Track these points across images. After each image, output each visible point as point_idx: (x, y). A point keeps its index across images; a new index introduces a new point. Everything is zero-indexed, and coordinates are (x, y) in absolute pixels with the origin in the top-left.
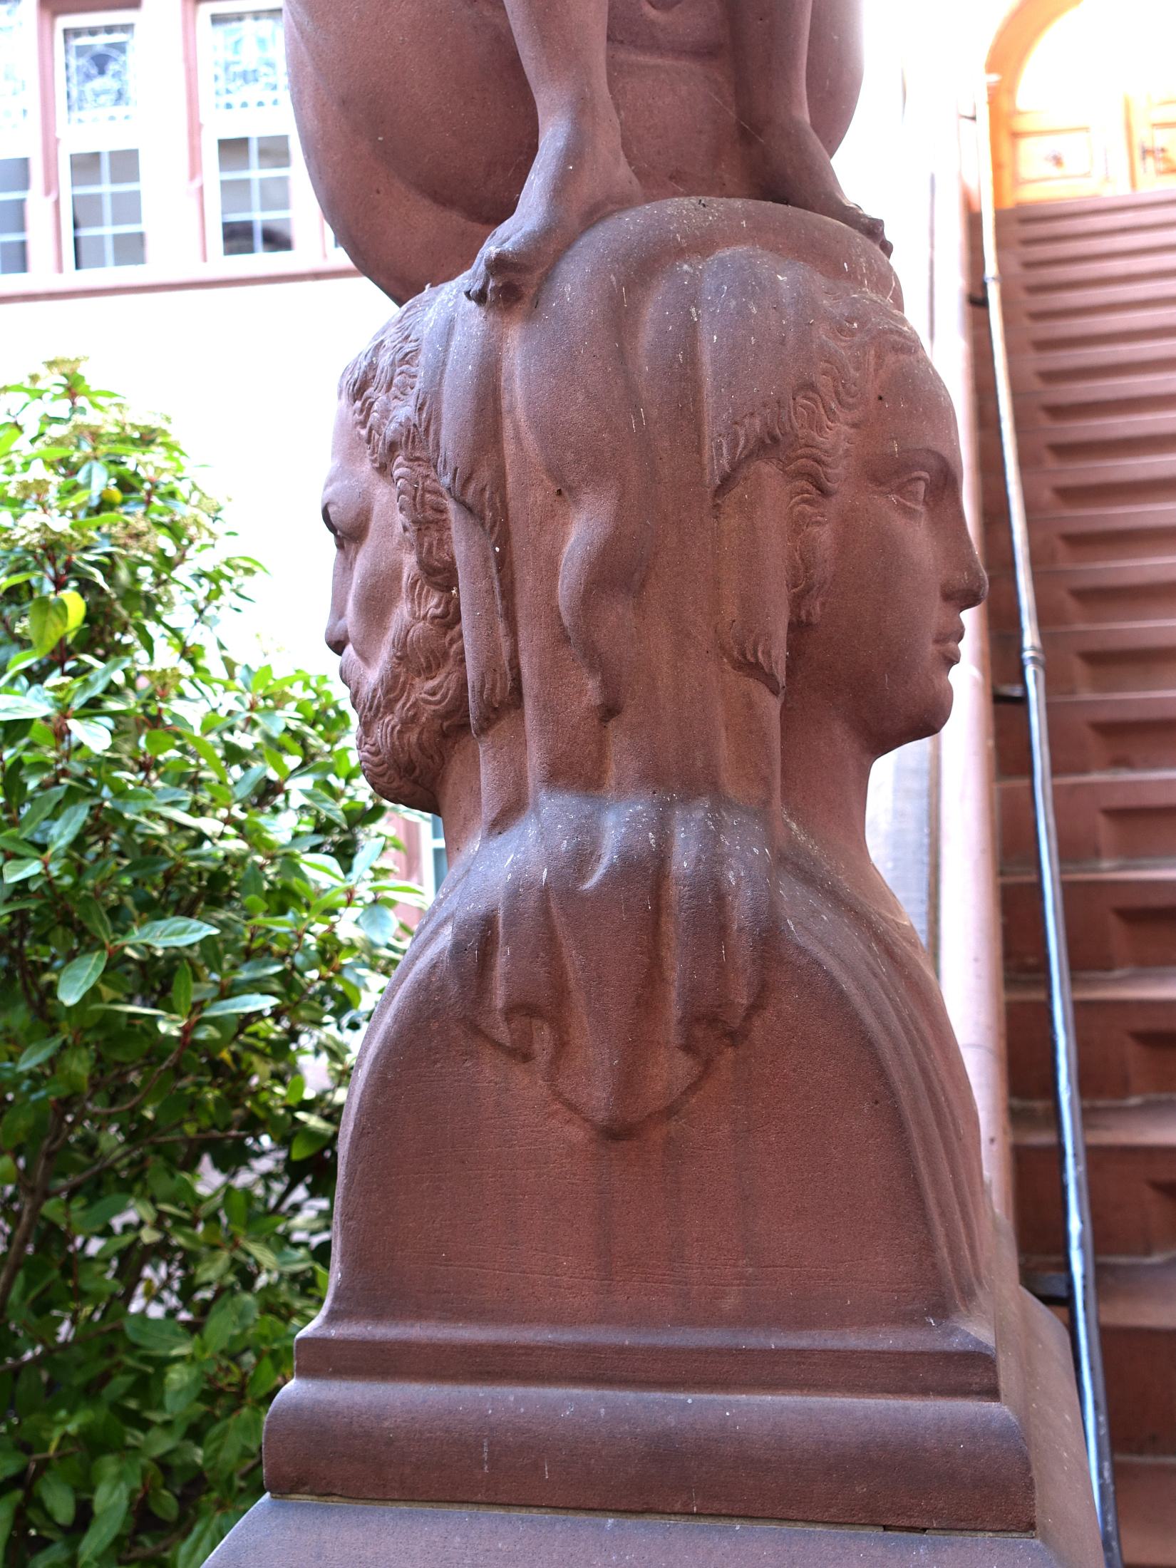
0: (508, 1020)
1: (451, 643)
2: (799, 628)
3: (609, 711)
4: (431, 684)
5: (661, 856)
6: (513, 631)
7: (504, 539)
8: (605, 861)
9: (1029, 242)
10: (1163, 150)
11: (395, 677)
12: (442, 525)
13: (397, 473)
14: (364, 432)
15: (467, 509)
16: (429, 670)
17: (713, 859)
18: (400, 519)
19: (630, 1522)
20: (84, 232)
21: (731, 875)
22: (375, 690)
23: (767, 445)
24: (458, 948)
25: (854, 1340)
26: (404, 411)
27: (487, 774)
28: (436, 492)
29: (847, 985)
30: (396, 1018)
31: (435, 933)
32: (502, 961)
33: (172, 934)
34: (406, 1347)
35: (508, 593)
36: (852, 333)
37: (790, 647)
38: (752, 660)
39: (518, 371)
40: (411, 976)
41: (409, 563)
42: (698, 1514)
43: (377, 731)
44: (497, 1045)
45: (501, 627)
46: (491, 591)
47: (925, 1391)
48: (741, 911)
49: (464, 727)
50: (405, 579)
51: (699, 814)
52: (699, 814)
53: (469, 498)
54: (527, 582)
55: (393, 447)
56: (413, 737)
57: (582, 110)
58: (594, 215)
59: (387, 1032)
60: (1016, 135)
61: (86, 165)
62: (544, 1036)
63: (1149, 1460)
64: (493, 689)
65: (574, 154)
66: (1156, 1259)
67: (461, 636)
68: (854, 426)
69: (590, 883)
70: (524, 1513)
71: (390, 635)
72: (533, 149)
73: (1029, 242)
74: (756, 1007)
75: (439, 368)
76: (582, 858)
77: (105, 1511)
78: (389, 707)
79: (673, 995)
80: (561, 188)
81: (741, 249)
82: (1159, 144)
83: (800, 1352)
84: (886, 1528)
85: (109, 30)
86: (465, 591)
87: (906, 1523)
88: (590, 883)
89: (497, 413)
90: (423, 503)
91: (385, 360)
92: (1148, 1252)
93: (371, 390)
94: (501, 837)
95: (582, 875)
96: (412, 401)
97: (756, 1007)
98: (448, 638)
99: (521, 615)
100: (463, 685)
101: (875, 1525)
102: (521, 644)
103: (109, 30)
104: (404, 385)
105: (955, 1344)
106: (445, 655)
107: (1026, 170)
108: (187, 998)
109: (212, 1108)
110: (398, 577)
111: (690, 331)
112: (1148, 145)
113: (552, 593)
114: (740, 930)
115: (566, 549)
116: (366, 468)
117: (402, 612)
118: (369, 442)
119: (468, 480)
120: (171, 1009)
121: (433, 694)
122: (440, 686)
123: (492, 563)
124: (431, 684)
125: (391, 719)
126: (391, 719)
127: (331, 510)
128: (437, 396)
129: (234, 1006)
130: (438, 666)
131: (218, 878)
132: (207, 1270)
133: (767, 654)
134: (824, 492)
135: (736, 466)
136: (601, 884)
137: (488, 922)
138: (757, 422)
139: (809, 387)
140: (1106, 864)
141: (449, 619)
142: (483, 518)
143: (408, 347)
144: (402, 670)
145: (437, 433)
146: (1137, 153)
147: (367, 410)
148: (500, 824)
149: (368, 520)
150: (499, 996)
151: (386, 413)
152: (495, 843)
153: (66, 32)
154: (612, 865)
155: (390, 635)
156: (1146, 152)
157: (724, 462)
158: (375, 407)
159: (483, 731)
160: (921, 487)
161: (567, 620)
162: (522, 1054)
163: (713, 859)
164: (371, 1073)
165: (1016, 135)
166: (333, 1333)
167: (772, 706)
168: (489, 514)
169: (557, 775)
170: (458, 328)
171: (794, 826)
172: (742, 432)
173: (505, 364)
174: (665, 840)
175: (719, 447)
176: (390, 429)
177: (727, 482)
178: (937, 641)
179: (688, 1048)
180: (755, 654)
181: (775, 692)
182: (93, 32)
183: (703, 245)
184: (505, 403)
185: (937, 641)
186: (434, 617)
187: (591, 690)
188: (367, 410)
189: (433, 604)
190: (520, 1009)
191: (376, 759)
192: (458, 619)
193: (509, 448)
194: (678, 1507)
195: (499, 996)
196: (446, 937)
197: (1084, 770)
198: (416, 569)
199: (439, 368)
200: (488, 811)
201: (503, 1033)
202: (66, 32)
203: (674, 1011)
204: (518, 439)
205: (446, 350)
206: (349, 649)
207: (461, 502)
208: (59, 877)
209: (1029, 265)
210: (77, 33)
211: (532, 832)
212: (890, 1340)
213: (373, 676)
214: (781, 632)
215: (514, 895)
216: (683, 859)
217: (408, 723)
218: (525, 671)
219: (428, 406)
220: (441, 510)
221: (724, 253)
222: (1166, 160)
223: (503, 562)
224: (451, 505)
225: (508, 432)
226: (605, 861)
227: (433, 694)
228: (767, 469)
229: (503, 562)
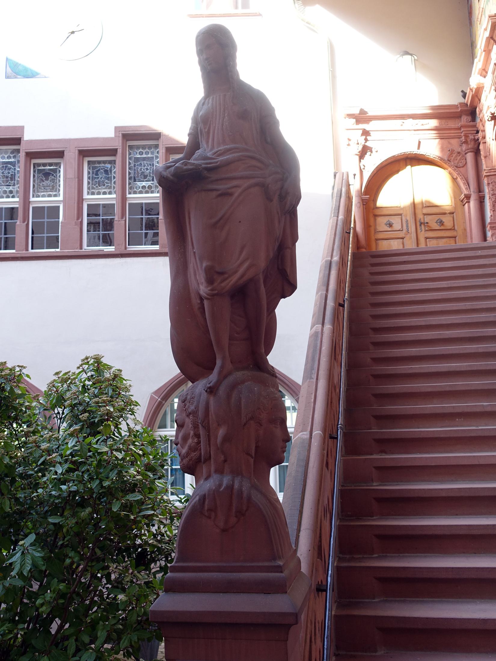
0: (207, 512)
1: (199, 447)
2: (257, 447)
3: (225, 461)
4: (195, 453)
5: (233, 486)
6: (210, 447)
7: (209, 432)
8: (224, 486)
9: (373, 265)
10: (427, 223)
11: (188, 452)
12: (198, 428)
13: (191, 418)
14: (184, 409)
15: (203, 426)
16: (194, 451)
17: (241, 486)
18: (191, 426)
19: (225, 594)
20: (34, 235)
21: (244, 489)
22: (184, 454)
23: (252, 418)
24: (200, 500)
25: (260, 564)
26: (192, 408)
27: (205, 470)
28: (198, 422)
29: (261, 507)
30: (189, 511)
31: (195, 497)
32: (206, 503)
33: (133, 497)
34: (188, 567)
35: (209, 441)
36: (267, 398)
37: (255, 450)
38: (248, 453)
39: (212, 405)
40: (191, 505)
41: (192, 433)
42: (236, 592)
43: (184, 461)
44: (205, 516)
45: (208, 446)
46: (206, 440)
47: (271, 572)
48: (245, 495)
49: (200, 461)
50: (191, 435)
51: (239, 478)
52: (239, 478)
53: (203, 425)
54: (212, 439)
55: (190, 414)
56: (191, 463)
57: (224, 358)
58: (225, 377)
59: (187, 514)
60: (376, 216)
61: (38, 211)
62: (213, 514)
63: (369, 654)
64: (206, 456)
65: (222, 367)
66: (376, 600)
67: (201, 446)
68: (267, 413)
69: (222, 489)
70: (208, 593)
71: (188, 445)
72: (215, 364)
73: (373, 265)
74: (247, 510)
75: (198, 402)
76: (220, 485)
77: (99, 637)
78: (187, 457)
79: (234, 508)
80: (220, 373)
81: (249, 383)
82: (426, 221)
83: (252, 566)
84: (265, 593)
85: (50, 164)
86: (202, 439)
87: (267, 592)
88: (222, 489)
89: (208, 410)
90: (195, 423)
91: (189, 397)
92: (374, 599)
93: (186, 402)
94: (207, 481)
95: (220, 488)
96: (194, 406)
97: (247, 510)
98: (198, 446)
99: (211, 444)
100: (201, 454)
101: (263, 593)
102: (211, 449)
103: (50, 164)
104: (192, 403)
105: (276, 564)
106: (198, 449)
107: (380, 228)
108: (136, 511)
109: (132, 538)
110: (190, 435)
111: (240, 399)
112: (422, 221)
113: (216, 441)
114: (245, 498)
115: (219, 434)
116: (184, 415)
117: (190, 441)
118: (185, 411)
119: (203, 422)
120: (132, 514)
121: (195, 455)
122: (196, 454)
123: (207, 435)
124: (195, 453)
125: (187, 459)
126: (187, 459)
127: (177, 421)
128: (198, 406)
129: (145, 513)
130: (196, 451)
131: (135, 485)
132: (126, 579)
133: (251, 452)
134: (261, 425)
135: (247, 422)
136: (223, 490)
137: (205, 495)
138: (250, 415)
139: (259, 409)
140: (375, 484)
141: (199, 443)
142: (205, 428)
143: (193, 396)
144: (189, 451)
145: (198, 413)
146: (418, 224)
147: (185, 405)
148: (206, 479)
149: (184, 424)
150: (206, 507)
151: (189, 407)
152: (206, 482)
153: (34, 164)
154: (225, 487)
155: (188, 445)
156: (421, 224)
157: (245, 421)
158: (187, 405)
159: (204, 463)
160: (279, 423)
161: (219, 446)
162: (209, 517)
163: (241, 486)
164: (184, 521)
165: (376, 216)
166: (176, 565)
167: (252, 461)
168: (207, 428)
169: (216, 471)
170: (202, 395)
171: (256, 480)
172: (248, 416)
173: (210, 403)
174: (233, 482)
175: (244, 418)
176: (190, 410)
177: (245, 424)
178: (281, 448)
179: (236, 517)
180: (249, 452)
181: (252, 458)
182: (44, 165)
183: (243, 382)
184: (210, 409)
185: (281, 448)
186: (196, 442)
187: (222, 458)
188: (185, 405)
189: (196, 440)
190: (209, 510)
191: (183, 466)
192: (200, 443)
193: (210, 417)
194: (232, 591)
195: (206, 507)
196: (197, 498)
197: (372, 454)
198: (193, 434)
199: (198, 402)
200: (204, 477)
201: (206, 514)
202: (34, 164)
203: (234, 510)
204: (212, 416)
205: (200, 399)
206: (179, 445)
207: (202, 425)
208: (111, 485)
209: (372, 274)
210: (39, 165)
211: (212, 481)
212: (266, 564)
213: (184, 451)
214: (254, 448)
215: (209, 491)
216: (236, 486)
217: (190, 460)
218: (212, 453)
219: (197, 407)
220: (198, 425)
221: (246, 384)
222: (428, 226)
223: (209, 436)
224: (200, 425)
225: (210, 414)
226: (224, 486)
227: (195, 455)
228: (252, 422)
229: (209, 436)
